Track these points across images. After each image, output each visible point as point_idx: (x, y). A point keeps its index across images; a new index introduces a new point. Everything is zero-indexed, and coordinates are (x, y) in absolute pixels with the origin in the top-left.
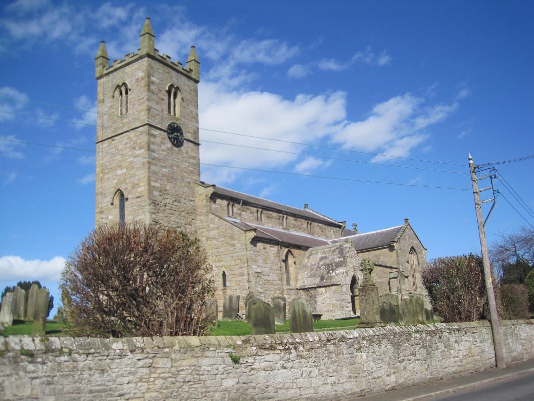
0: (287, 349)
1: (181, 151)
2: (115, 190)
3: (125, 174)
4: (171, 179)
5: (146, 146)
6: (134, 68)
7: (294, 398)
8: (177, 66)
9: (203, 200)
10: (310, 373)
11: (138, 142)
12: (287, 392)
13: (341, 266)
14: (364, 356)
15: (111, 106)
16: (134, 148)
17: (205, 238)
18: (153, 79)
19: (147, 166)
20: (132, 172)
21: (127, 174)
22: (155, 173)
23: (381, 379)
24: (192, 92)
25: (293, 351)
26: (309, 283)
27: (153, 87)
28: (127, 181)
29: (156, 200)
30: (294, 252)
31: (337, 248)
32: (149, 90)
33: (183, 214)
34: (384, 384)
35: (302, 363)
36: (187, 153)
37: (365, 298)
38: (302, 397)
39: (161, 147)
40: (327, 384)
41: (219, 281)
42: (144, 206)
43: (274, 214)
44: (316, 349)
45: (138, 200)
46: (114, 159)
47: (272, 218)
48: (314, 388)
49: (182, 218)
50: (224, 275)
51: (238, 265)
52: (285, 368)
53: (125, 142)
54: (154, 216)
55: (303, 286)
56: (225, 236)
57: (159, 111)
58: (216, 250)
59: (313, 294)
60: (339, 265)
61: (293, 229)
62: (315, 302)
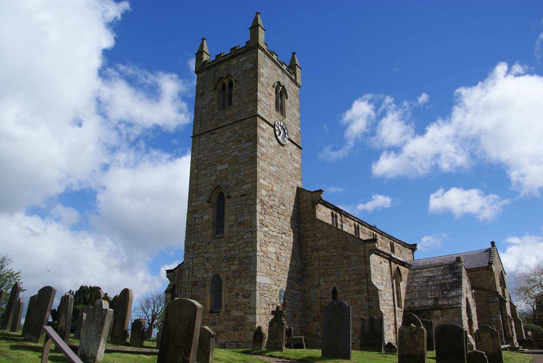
2: (212, 187)
3: (227, 169)
6: (241, 60)
11: (245, 134)
15: (212, 99)
16: (240, 141)
17: (309, 249)
20: (236, 167)
28: (230, 177)
41: (328, 298)
42: (251, 205)
45: (243, 198)
46: (213, 153)
51: (353, 280)
53: (228, 135)
56: (337, 247)
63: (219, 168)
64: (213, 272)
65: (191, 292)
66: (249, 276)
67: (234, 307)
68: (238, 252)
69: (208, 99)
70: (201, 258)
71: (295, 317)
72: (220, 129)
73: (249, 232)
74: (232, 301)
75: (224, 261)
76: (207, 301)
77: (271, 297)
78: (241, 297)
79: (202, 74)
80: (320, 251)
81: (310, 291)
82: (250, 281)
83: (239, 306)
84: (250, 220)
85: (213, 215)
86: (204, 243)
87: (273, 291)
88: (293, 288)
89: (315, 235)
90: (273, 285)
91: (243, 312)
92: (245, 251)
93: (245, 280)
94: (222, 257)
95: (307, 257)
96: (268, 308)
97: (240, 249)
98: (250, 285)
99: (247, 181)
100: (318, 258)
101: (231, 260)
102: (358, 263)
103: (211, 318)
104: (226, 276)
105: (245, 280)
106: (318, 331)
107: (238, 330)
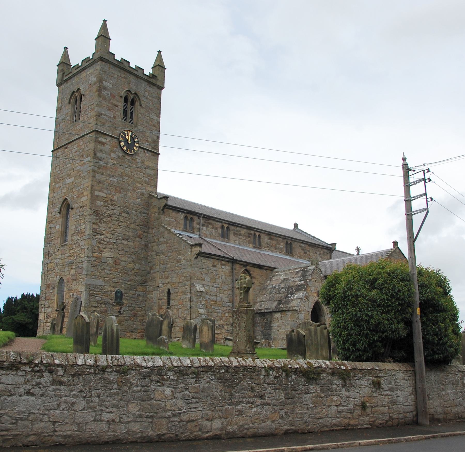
0: (38, 371)
1: (134, 160)
4: (119, 189)
5: (92, 153)
7: (43, 433)
8: (137, 71)
9: (156, 213)
10: (73, 404)
12: (33, 424)
13: (300, 290)
14: (168, 391)
17: (154, 253)
18: (105, 84)
19: (91, 174)
21: (74, 183)
22: (100, 182)
23: (195, 423)
24: (154, 100)
25: (46, 374)
26: (265, 307)
27: (104, 92)
28: (74, 190)
29: (99, 210)
30: (254, 272)
31: (301, 271)
32: (99, 95)
33: (132, 226)
34: (200, 430)
35: (60, 390)
36: (143, 162)
37: (238, 322)
38: (56, 434)
39: (110, 155)
40: (102, 421)
41: (164, 299)
43: (243, 231)
44: (86, 375)
47: (240, 235)
48: (78, 424)
49: (130, 230)
50: (169, 292)
52: (32, 394)
54: (95, 226)
55: (260, 310)
57: (111, 117)
58: (163, 266)
59: (269, 319)
60: (299, 288)
61: (267, 249)
62: (270, 328)
63: (68, 181)
65: (45, 293)
69: (64, 113)
70: (53, 264)
72: (71, 144)
75: (67, 265)
79: (62, 86)
84: (84, 230)
99: (84, 194)
102: (186, 266)
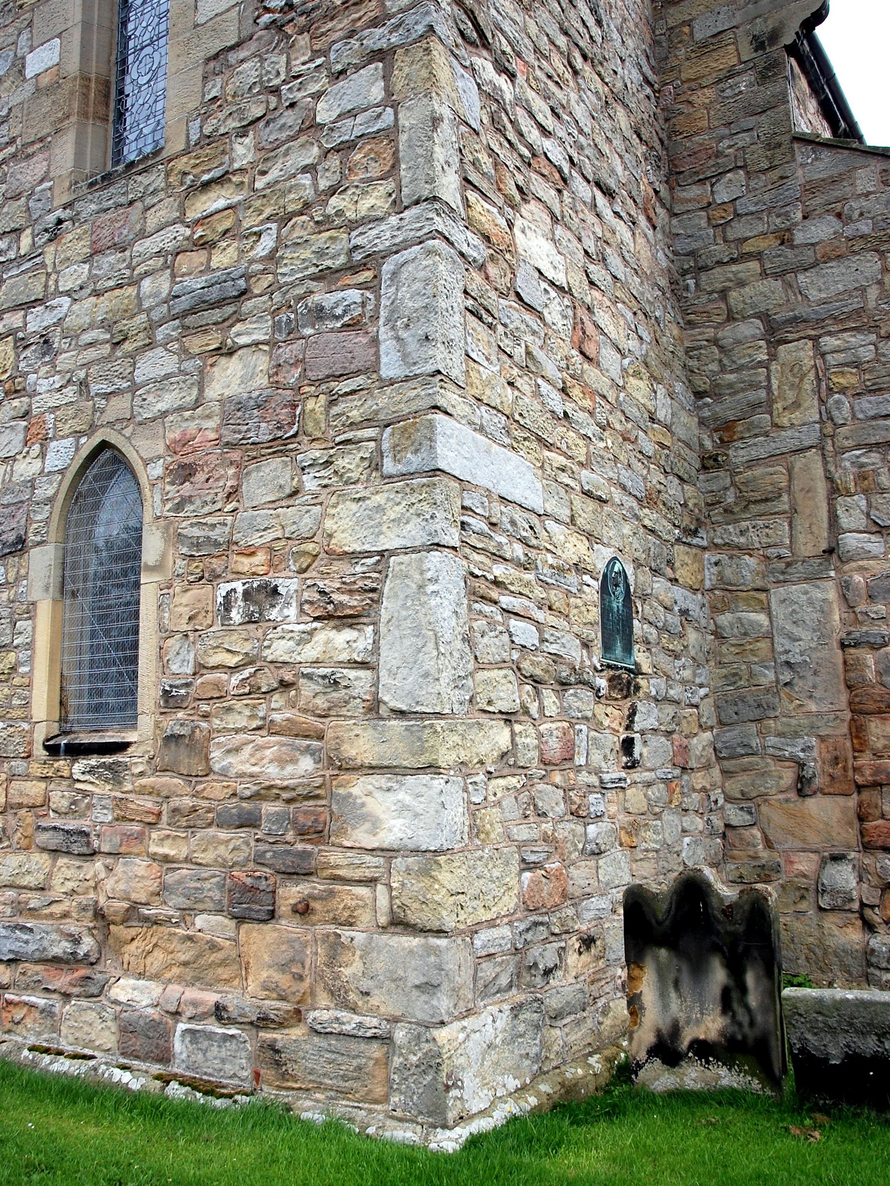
17: (751, 328)
64: (78, 434)
66: (368, 422)
67: (238, 705)
68: (267, 243)
71: (684, 769)
73: (358, 68)
74: (220, 658)
75: (160, 334)
76: (31, 660)
77: (552, 620)
78: (292, 611)
80: (830, 334)
81: (762, 596)
82: (378, 467)
83: (277, 700)
85: (86, 26)
86: (26, 241)
87: (560, 570)
88: (669, 572)
89: (785, 238)
90: (557, 521)
91: (307, 750)
92: (321, 225)
93: (328, 463)
94: (146, 305)
95: (731, 377)
96: (534, 708)
97: (285, 219)
98: (379, 499)
100: (819, 380)
101: (217, 315)
103: (60, 798)
104: (171, 449)
105: (328, 463)
106: (837, 858)
107: (272, 915)
